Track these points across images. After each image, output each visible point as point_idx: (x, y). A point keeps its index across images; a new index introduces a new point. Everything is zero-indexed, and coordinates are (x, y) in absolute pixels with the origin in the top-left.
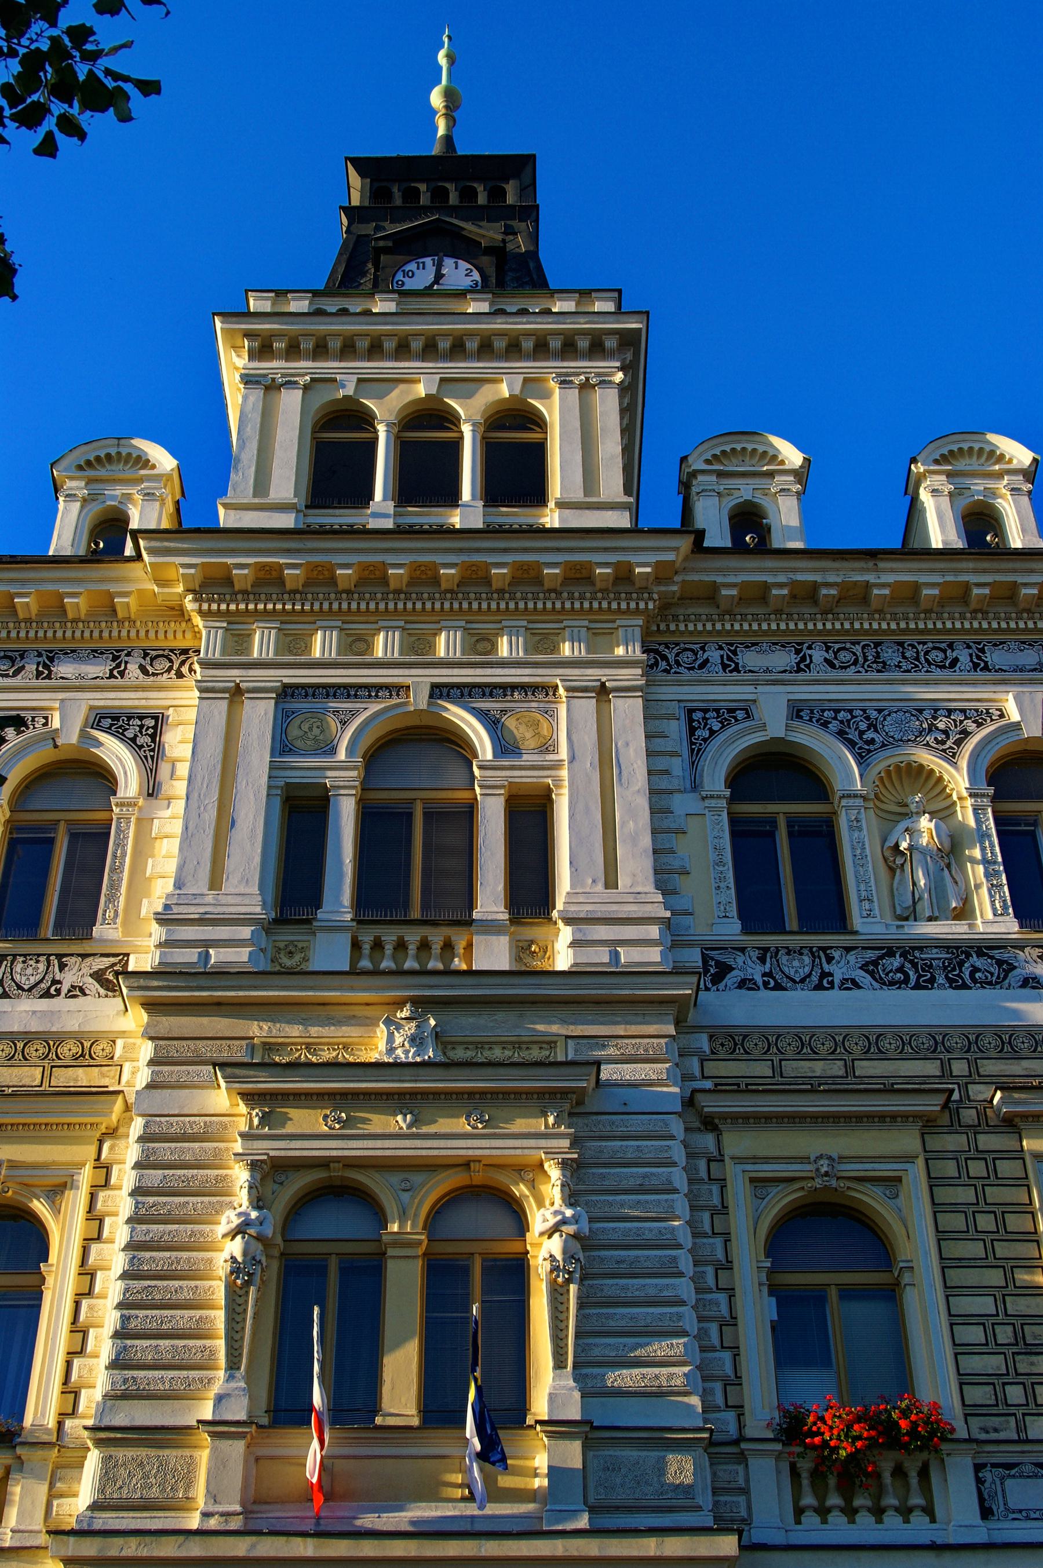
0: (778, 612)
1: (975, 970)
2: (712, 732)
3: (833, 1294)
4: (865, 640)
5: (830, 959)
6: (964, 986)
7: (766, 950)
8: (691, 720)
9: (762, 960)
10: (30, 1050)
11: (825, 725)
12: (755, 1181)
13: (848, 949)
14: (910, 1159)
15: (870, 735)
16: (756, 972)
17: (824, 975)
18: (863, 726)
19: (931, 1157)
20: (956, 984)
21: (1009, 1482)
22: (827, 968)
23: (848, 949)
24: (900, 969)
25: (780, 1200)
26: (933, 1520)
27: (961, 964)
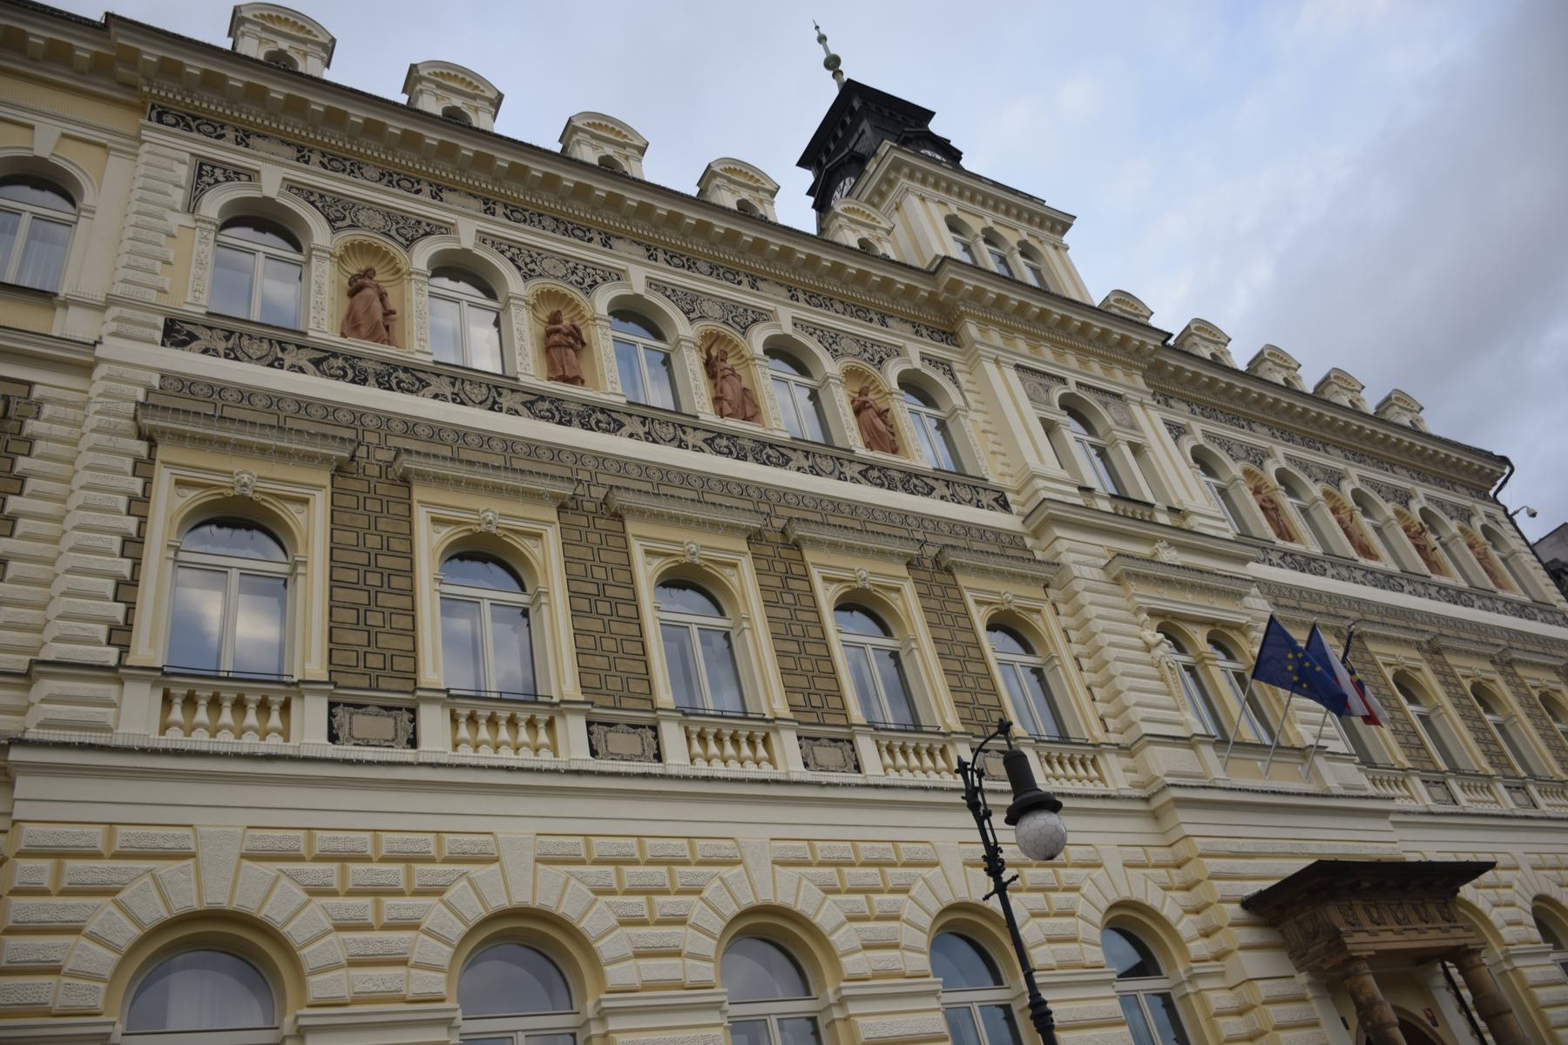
0: (625, 217)
1: (598, 421)
2: (217, 181)
3: (486, 605)
4: (532, 209)
5: (500, 395)
6: (390, 389)
7: (232, 333)
8: (201, 169)
9: (227, 339)
10: (349, 418)
11: (502, 252)
12: (435, 521)
13: (299, 347)
14: (320, 487)
15: (532, 266)
16: (448, 391)
17: (495, 402)
18: (528, 260)
19: (756, 557)
20: (585, 426)
21: (610, 735)
22: (280, 355)
23: (299, 347)
24: (343, 369)
25: (192, 498)
26: (556, 755)
27: (390, 375)
